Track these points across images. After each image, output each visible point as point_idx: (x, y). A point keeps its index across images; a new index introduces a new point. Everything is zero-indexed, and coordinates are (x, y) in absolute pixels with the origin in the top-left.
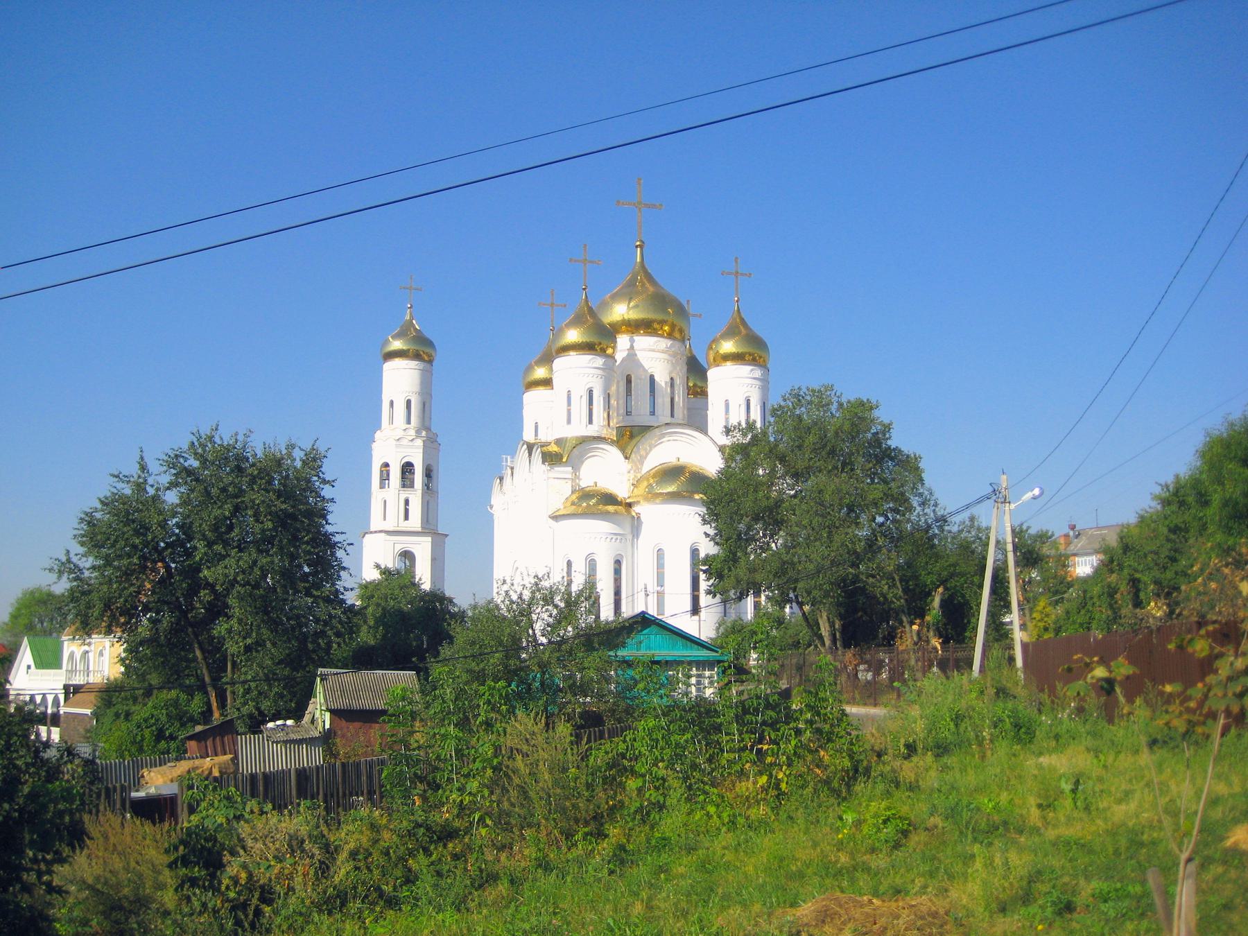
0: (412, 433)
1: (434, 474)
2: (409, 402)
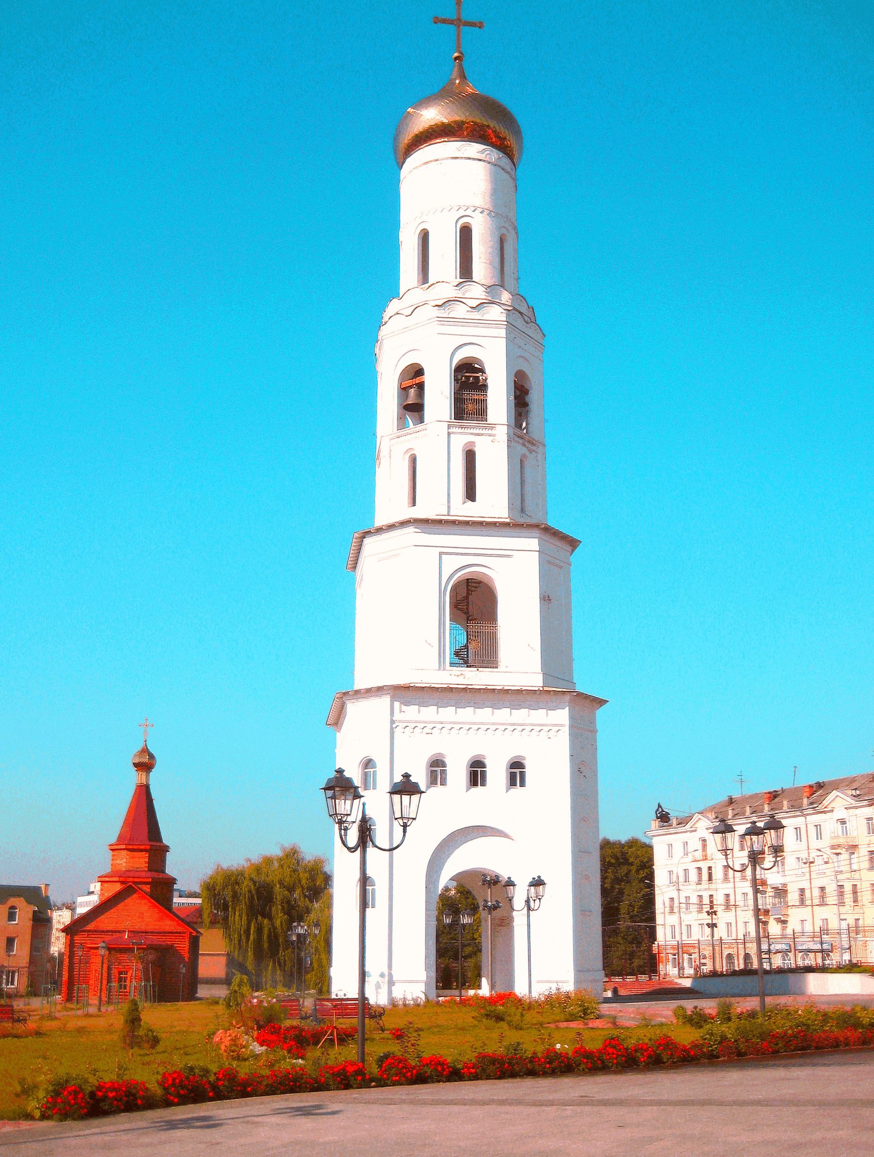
1: (533, 398)
2: (466, 234)
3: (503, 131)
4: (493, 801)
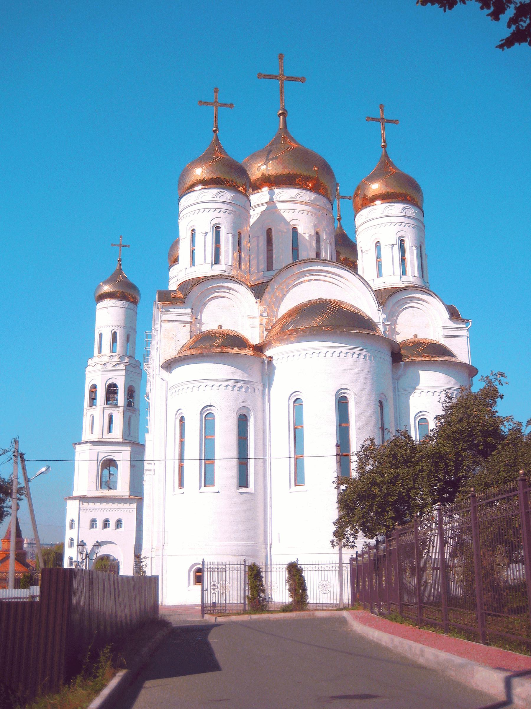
0: (116, 359)
1: (136, 395)
3: (132, 292)
4: (110, 534)
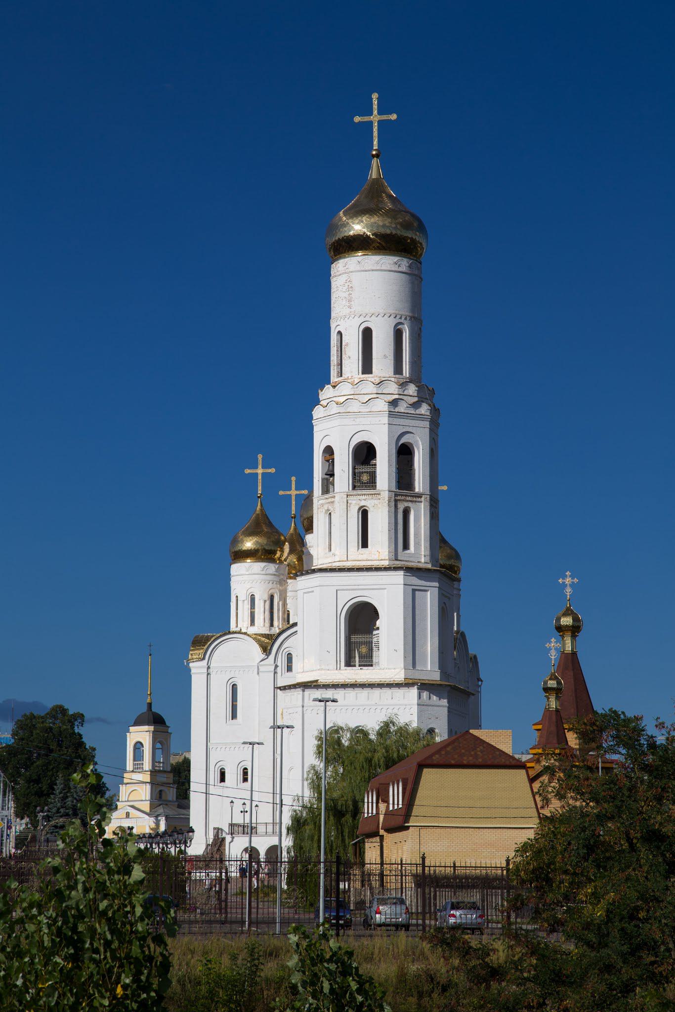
2: (367, 334)
